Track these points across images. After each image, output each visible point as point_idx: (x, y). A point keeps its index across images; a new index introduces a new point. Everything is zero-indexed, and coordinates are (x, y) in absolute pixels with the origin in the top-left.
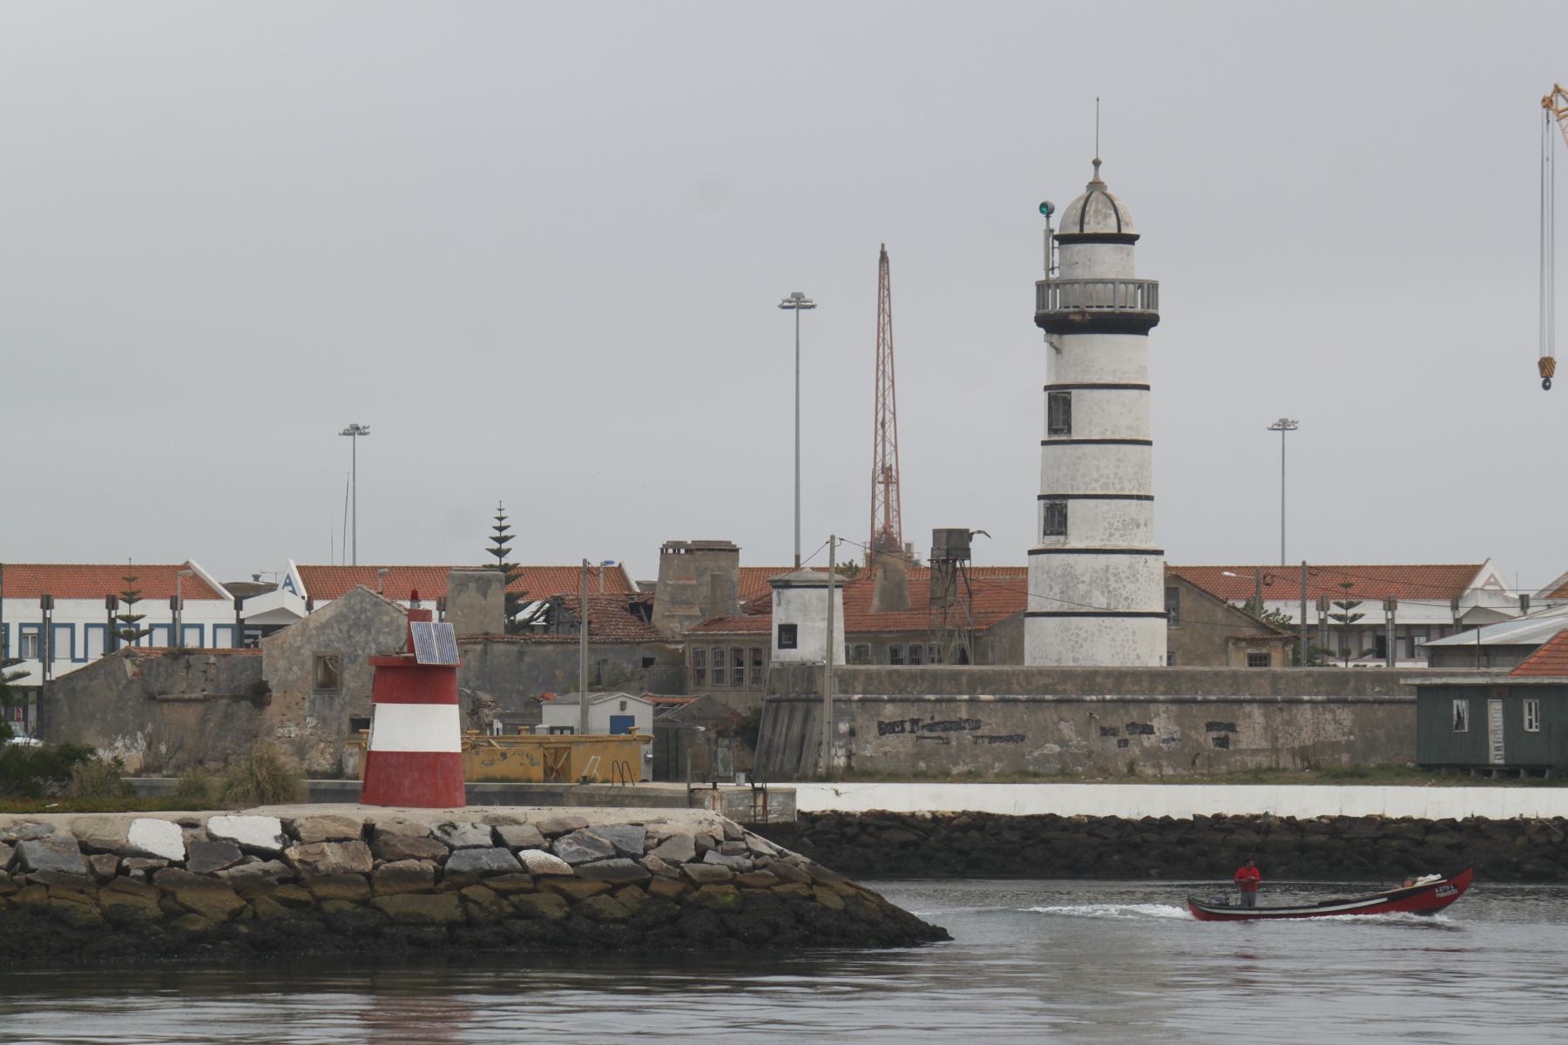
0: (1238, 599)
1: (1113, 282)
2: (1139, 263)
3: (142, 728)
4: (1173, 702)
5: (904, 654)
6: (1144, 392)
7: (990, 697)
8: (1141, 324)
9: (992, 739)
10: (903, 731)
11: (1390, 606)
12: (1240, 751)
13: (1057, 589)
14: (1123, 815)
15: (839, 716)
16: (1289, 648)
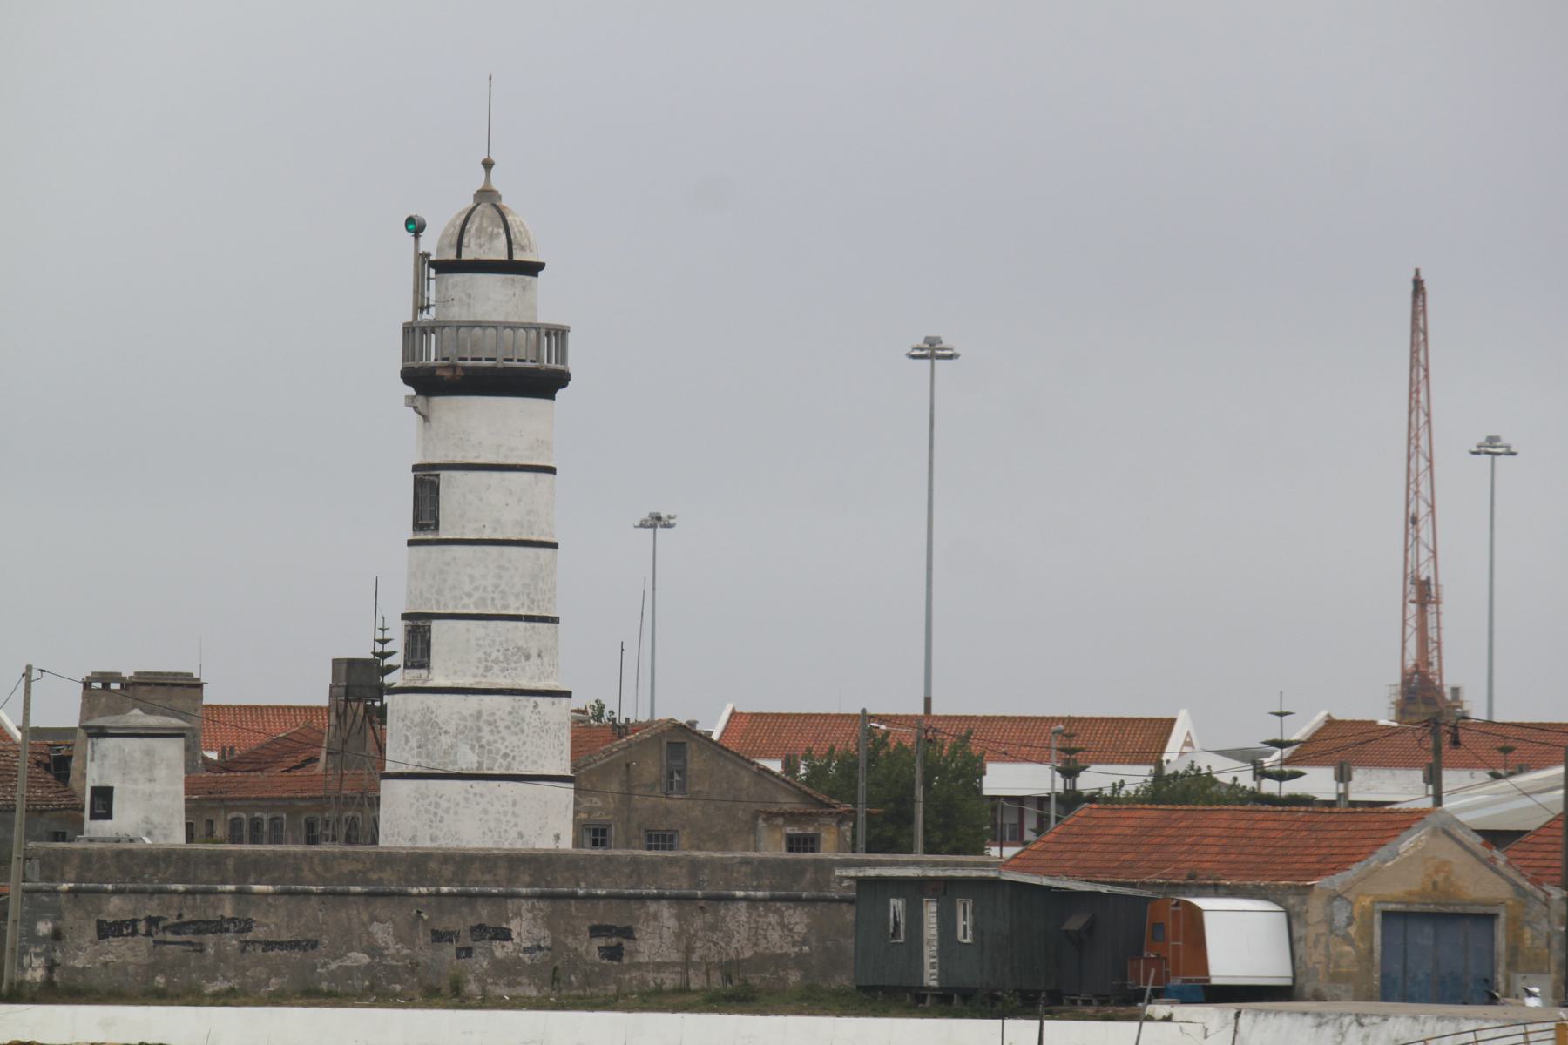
0: (211, 750)
1: (494, 325)
2: (545, 301)
4: (542, 897)
5: (220, 830)
6: (548, 477)
7: (269, 888)
8: (544, 383)
9: (269, 945)
10: (134, 933)
11: (1343, 776)
12: (639, 966)
13: (413, 743)
16: (847, 828)
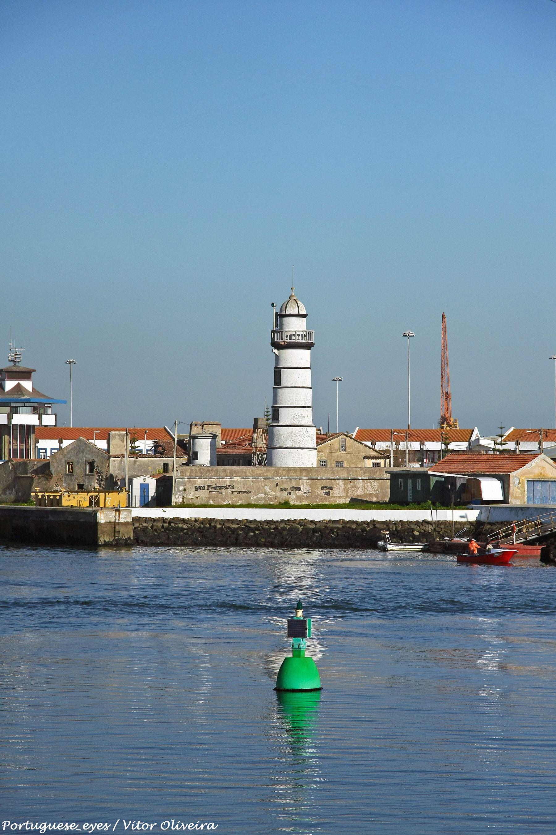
3: (14, 487)
9: (238, 492)
10: (204, 489)
12: (334, 497)
14: (258, 519)
15: (180, 484)
